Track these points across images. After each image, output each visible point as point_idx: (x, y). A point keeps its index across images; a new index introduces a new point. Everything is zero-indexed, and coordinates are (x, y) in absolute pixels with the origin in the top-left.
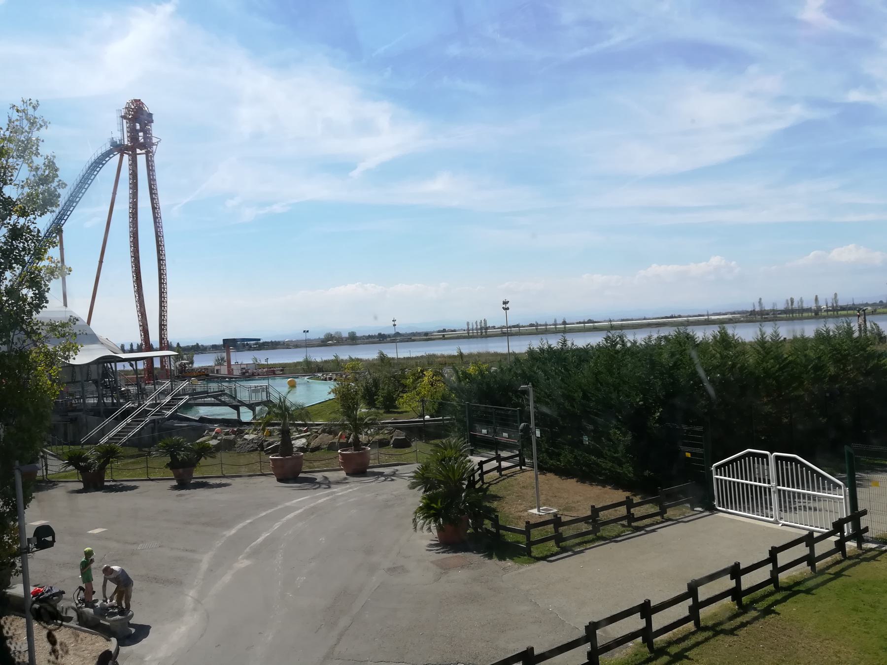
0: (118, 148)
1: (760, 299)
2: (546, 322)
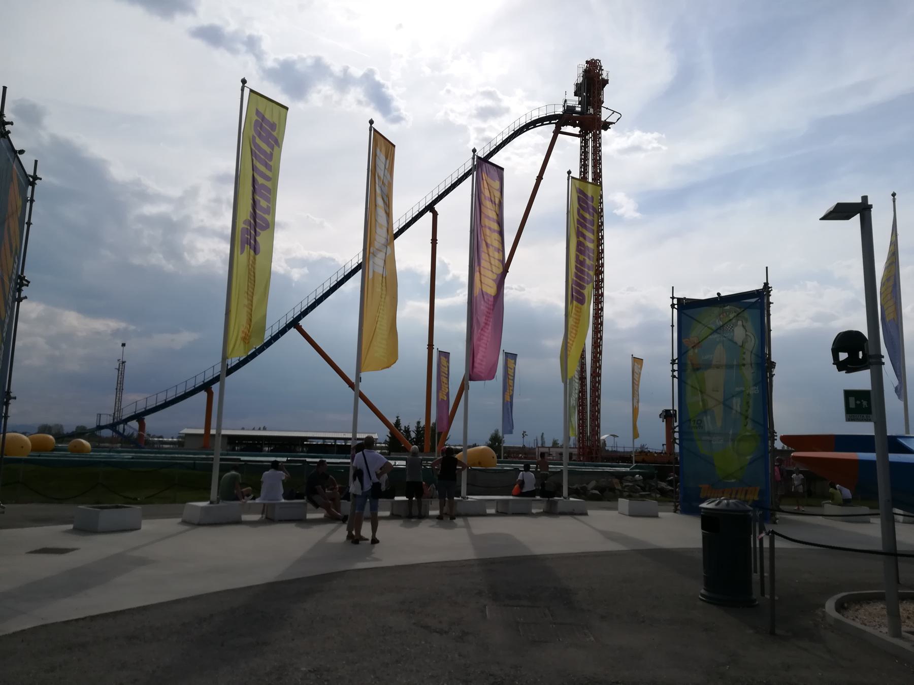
0: (561, 120)
1: (543, 434)
2: (718, 294)
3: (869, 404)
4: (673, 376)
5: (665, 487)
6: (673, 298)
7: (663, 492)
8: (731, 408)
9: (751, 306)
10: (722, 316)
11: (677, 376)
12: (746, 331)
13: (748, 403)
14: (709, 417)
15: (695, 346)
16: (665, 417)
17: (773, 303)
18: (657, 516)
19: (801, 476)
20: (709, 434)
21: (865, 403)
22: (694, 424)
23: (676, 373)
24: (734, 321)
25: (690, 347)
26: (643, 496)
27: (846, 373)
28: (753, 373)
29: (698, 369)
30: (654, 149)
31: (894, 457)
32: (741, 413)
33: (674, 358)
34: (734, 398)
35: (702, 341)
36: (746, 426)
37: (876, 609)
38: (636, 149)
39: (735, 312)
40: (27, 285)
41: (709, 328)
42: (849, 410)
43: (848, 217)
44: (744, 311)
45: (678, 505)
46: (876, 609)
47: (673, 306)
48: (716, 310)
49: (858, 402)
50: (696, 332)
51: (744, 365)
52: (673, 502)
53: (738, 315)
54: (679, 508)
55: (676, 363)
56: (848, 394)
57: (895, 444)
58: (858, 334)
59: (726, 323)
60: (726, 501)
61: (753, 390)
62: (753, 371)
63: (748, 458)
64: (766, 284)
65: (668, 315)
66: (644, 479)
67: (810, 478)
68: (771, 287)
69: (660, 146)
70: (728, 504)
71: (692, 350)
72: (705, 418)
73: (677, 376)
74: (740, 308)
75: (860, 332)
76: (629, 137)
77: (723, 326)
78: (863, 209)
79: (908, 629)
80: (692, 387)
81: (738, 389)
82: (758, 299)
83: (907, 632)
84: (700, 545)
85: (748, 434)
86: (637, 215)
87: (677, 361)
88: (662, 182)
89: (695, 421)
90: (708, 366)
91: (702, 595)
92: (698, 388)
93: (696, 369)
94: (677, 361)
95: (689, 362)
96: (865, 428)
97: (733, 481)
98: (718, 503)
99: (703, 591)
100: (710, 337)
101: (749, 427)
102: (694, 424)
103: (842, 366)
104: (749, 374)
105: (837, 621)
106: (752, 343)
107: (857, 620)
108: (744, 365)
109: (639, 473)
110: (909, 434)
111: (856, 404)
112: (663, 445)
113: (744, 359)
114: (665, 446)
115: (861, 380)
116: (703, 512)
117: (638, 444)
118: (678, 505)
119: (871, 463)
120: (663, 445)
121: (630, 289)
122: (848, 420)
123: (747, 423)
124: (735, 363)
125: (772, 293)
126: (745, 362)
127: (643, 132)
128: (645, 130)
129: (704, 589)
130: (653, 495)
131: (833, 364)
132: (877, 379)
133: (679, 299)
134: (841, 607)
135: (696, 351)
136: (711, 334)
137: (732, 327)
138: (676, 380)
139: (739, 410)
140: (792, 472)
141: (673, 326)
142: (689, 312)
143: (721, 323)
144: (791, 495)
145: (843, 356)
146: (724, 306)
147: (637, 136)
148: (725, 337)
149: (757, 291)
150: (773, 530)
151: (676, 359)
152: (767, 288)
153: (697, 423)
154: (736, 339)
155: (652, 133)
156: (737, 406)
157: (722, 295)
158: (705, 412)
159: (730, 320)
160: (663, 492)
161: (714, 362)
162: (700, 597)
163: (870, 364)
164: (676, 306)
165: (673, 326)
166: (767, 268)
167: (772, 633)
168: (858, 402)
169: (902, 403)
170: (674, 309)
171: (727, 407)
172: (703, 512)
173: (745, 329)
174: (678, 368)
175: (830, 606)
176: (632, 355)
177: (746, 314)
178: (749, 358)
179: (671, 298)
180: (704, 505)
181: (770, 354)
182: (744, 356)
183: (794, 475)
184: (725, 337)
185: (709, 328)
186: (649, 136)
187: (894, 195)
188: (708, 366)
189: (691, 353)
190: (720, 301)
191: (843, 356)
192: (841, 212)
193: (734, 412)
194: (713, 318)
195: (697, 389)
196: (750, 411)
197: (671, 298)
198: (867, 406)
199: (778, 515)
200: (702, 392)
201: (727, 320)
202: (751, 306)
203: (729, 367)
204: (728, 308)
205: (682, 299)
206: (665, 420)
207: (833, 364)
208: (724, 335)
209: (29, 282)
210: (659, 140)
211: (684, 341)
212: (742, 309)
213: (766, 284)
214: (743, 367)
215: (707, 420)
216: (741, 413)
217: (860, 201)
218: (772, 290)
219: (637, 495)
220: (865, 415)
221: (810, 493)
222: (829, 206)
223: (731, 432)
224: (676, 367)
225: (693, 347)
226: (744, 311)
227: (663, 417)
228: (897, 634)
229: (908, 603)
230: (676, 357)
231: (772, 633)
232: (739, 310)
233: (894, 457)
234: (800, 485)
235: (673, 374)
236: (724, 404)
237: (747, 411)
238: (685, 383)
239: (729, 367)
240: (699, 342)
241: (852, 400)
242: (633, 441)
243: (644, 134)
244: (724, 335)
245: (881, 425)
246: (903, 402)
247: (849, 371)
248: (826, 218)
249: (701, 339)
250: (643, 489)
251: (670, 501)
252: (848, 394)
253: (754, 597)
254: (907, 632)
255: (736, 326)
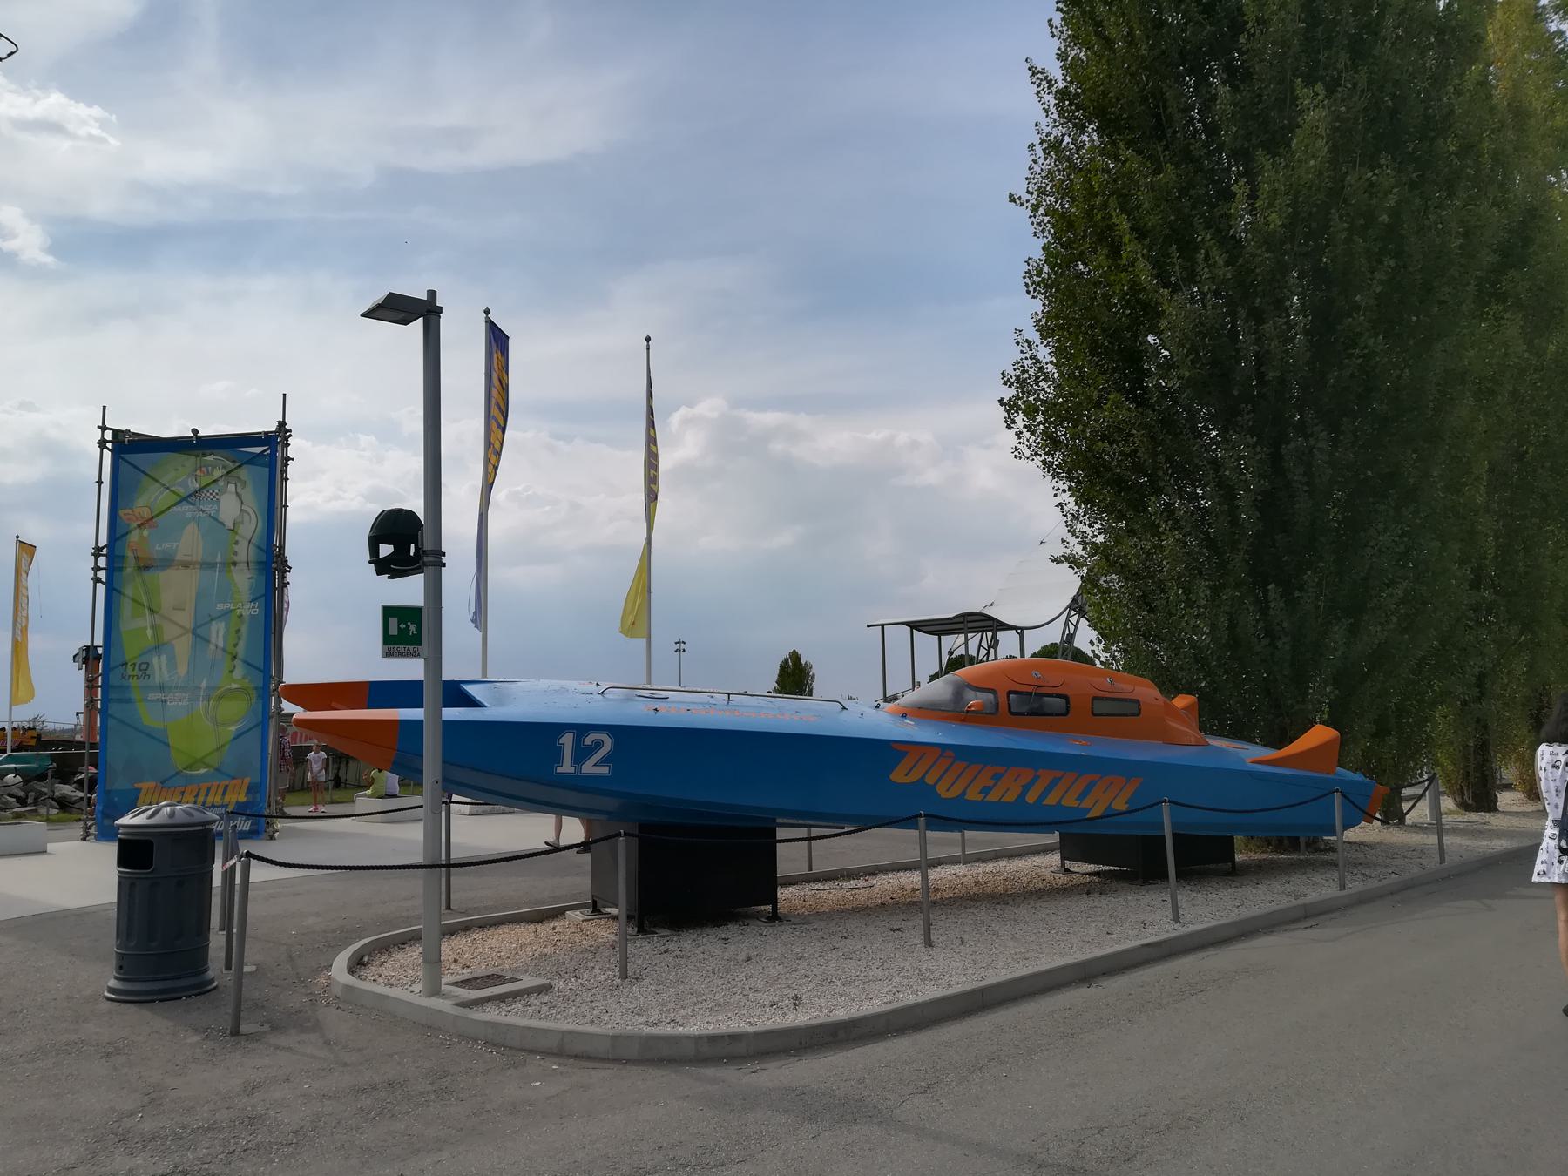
2: (195, 431)
3: (419, 629)
4: (97, 580)
5: (69, 794)
6: (103, 428)
7: (64, 804)
8: (208, 641)
9: (253, 460)
10: (198, 473)
11: (104, 580)
12: (242, 503)
13: (238, 631)
14: (163, 658)
15: (142, 524)
16: (86, 660)
17: (293, 459)
18: (44, 852)
19: (323, 754)
20: (162, 688)
21: (413, 627)
22: (133, 670)
23: (102, 575)
24: (221, 483)
25: (135, 525)
26: (18, 816)
27: (389, 578)
28: (250, 578)
29: (147, 568)
30: (91, 137)
31: (451, 714)
32: (224, 650)
33: (100, 545)
34: (214, 623)
35: (157, 515)
36: (231, 672)
37: (411, 956)
38: (52, 127)
39: (224, 467)
40: (289, 572)
41: (171, 491)
42: (388, 640)
43: (405, 322)
44: (240, 466)
45: (91, 826)
46: (411, 956)
47: (102, 443)
48: (187, 461)
49: (403, 626)
50: (150, 498)
51: (234, 564)
52: (80, 820)
53: (228, 473)
54: (93, 830)
55: (103, 555)
56: (388, 612)
57: (456, 694)
58: (410, 515)
59: (206, 486)
60: (168, 808)
61: (250, 610)
62: (250, 576)
63: (233, 728)
64: (282, 424)
65: (92, 463)
66: (26, 781)
67: (338, 759)
68: (290, 431)
69: (104, 135)
70: (172, 815)
71: (137, 530)
72: (155, 660)
73: (104, 580)
74: (234, 461)
75: (399, 511)
76: (36, 99)
77: (199, 491)
78: (424, 311)
79: (453, 979)
80: (134, 600)
81: (220, 607)
82: (267, 449)
83: (456, 984)
84: (114, 899)
85: (234, 686)
86: (49, 259)
87: (105, 551)
88: (101, 207)
89: (134, 664)
90: (167, 562)
91: (111, 990)
92: (145, 603)
93: (145, 567)
94: (105, 551)
95: (129, 554)
96: (410, 669)
97: (203, 771)
98: (153, 812)
99: (112, 983)
100: (175, 509)
101: (238, 674)
102: (133, 670)
103: (383, 567)
104: (244, 580)
105: (349, 989)
106: (252, 526)
107: (380, 980)
108: (234, 564)
109: (16, 771)
110: (486, 677)
111: (399, 628)
112: (78, 714)
113: (235, 553)
114: (81, 716)
115: (409, 590)
116: (122, 834)
117: (23, 715)
118: (91, 826)
119: (418, 724)
120: (78, 714)
121: (26, 406)
122: (386, 655)
123: (235, 667)
124: (219, 559)
125: (290, 441)
126: (236, 559)
127: (71, 98)
128: (76, 92)
129: (116, 978)
130: (43, 811)
131: (370, 562)
132: (434, 591)
133: (116, 433)
134: (357, 964)
135: (145, 533)
136: (177, 504)
137: (217, 494)
138: (101, 588)
139: (221, 644)
140: (309, 749)
141: (100, 482)
142: (136, 458)
143: (197, 486)
144: (300, 788)
145: (386, 550)
146: (204, 455)
147: (54, 103)
148: (203, 511)
149: (266, 433)
150: (248, 852)
151: (103, 548)
152: (283, 432)
153: (140, 669)
154: (222, 517)
155: (90, 105)
156: (217, 636)
157: (202, 433)
158: (158, 648)
159: (214, 481)
160: (64, 804)
161: (179, 557)
162: (106, 994)
163: (424, 564)
164: (109, 445)
165: (100, 482)
166: (285, 395)
167: (235, 1032)
168: (403, 626)
169: (480, 635)
170: (105, 450)
171: (199, 635)
172: (122, 834)
173: (240, 499)
174: (107, 565)
175: (339, 968)
176: (17, 537)
177: (244, 473)
178: (245, 551)
179: (99, 427)
180: (126, 820)
181: (282, 547)
182: (236, 548)
183: (311, 755)
184: (203, 511)
185: (171, 491)
186: (81, 110)
187: (648, 339)
188: (167, 562)
189: (134, 537)
190: (196, 445)
191: (386, 550)
192: (394, 309)
193: (212, 647)
194: (180, 473)
195: (144, 605)
196: (242, 644)
197: (99, 427)
198: (415, 633)
199: (279, 824)
200: (151, 610)
201: (206, 480)
202: (253, 460)
203: (207, 565)
204: (211, 458)
205: (122, 431)
206: (84, 666)
207: (370, 562)
208: (201, 507)
209: (290, 568)
210: (103, 124)
211: (121, 513)
212: (237, 464)
213: (282, 424)
214: (232, 568)
215: (159, 664)
216: (224, 650)
217: (425, 297)
218: (291, 436)
219: (8, 813)
220: (411, 647)
221: (338, 783)
222: (379, 296)
223: (204, 684)
224: (102, 562)
225: (139, 526)
226: (240, 466)
227: (81, 659)
228: (435, 991)
229: (459, 938)
230: (103, 541)
231: (235, 1032)
232: (231, 465)
233: (451, 714)
234: (321, 770)
235: (95, 574)
236: (194, 632)
237: (236, 645)
238: (119, 592)
239: (207, 565)
240: (153, 518)
241: (393, 621)
242: (11, 709)
243: (72, 102)
244: (201, 507)
245: (435, 664)
246: (481, 634)
247: (395, 575)
248: (367, 315)
249: (156, 513)
250: (22, 801)
251: (77, 821)
252: (388, 612)
253: (211, 974)
254: (456, 984)
255: (225, 492)
